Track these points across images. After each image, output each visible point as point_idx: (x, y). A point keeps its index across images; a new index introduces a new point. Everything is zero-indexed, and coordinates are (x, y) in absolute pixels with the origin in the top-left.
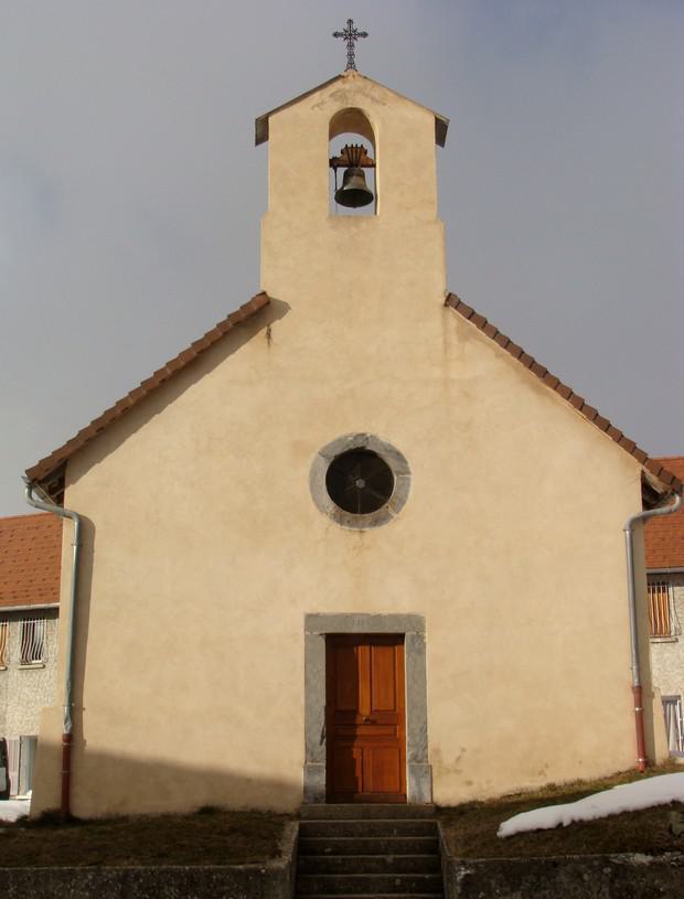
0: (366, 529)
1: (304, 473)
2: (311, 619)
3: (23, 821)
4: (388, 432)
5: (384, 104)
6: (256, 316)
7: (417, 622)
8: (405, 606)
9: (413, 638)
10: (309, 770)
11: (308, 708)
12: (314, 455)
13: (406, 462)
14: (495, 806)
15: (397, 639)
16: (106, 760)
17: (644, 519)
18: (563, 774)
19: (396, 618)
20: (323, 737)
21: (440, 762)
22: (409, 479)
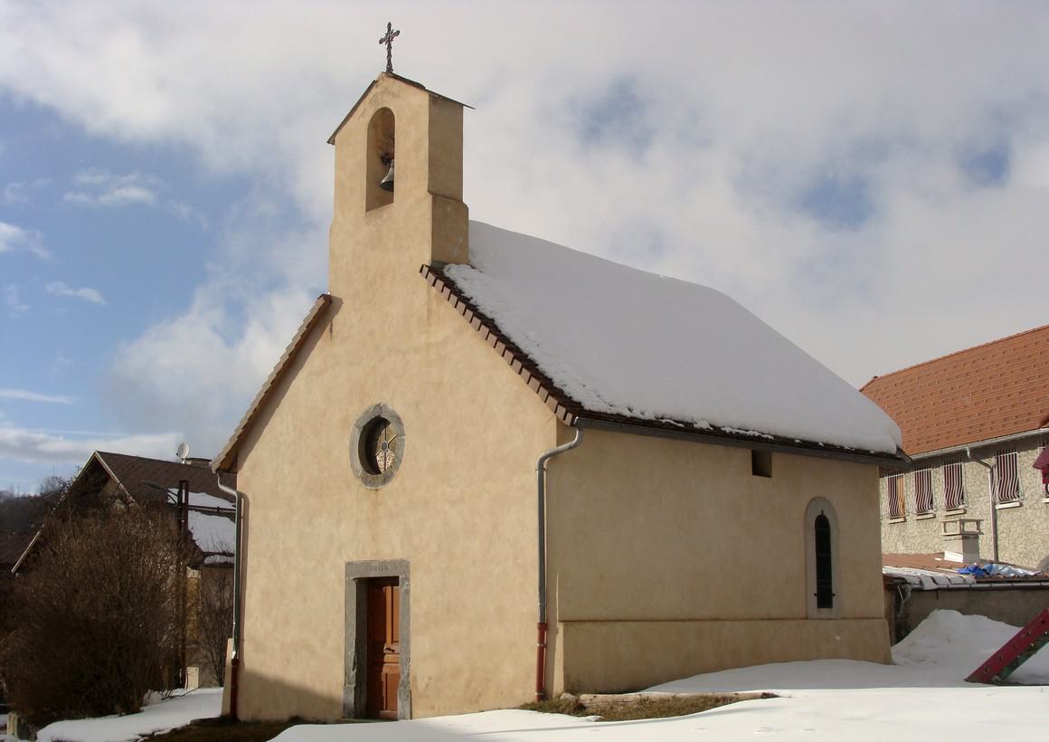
0: (380, 487)
1: (347, 442)
2: (349, 565)
3: (585, 693)
4: (396, 405)
5: (399, 97)
6: (331, 141)
7: (405, 564)
8: (399, 554)
9: (403, 579)
10: (346, 693)
11: (347, 640)
12: (351, 428)
13: (402, 425)
14: (156, 695)
15: (394, 581)
16: (260, 680)
17: (553, 456)
18: (161, 728)
19: (393, 562)
20: (354, 664)
21: (417, 688)
22: (404, 440)
